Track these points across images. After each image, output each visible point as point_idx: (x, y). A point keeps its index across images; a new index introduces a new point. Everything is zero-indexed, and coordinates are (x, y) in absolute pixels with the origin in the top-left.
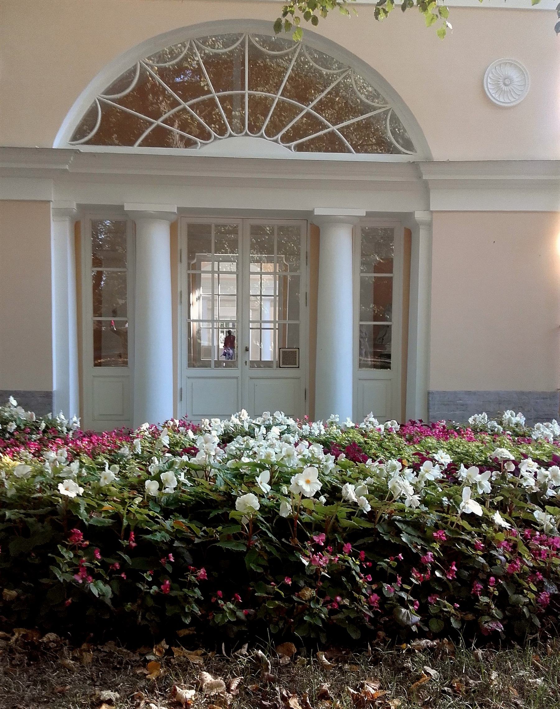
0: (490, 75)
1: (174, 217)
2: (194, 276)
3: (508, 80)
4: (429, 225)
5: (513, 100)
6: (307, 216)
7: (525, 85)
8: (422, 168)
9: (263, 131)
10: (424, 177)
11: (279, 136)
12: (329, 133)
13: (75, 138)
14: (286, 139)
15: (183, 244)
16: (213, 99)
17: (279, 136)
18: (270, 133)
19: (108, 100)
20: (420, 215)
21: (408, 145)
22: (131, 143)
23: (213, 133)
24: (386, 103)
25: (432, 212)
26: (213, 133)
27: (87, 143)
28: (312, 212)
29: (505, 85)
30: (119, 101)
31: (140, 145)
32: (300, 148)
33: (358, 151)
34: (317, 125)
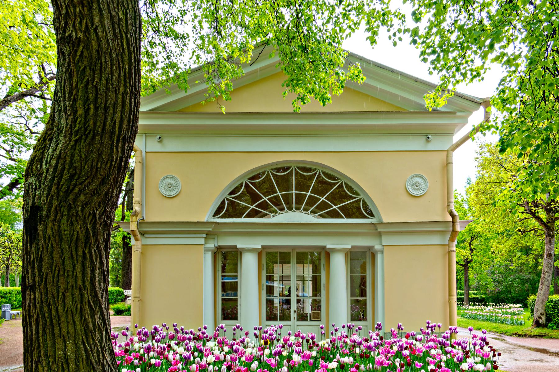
0: (162, 188)
1: (260, 251)
2: (270, 276)
3: (417, 184)
4: (382, 252)
5: (423, 191)
6: (324, 248)
7: (426, 183)
8: (378, 226)
9: (302, 209)
10: (379, 230)
11: (309, 211)
12: (333, 209)
13: (216, 214)
14: (313, 212)
15: (264, 262)
16: (278, 195)
17: (309, 211)
18: (305, 210)
19: (230, 197)
20: (378, 247)
21: (372, 215)
22: (240, 216)
23: (286, 209)
24: (359, 195)
25: (383, 246)
26: (286, 209)
27: (221, 217)
28: (325, 246)
29: (417, 186)
30: (233, 198)
31: (244, 218)
32: (322, 216)
33: (347, 218)
34: (327, 206)
